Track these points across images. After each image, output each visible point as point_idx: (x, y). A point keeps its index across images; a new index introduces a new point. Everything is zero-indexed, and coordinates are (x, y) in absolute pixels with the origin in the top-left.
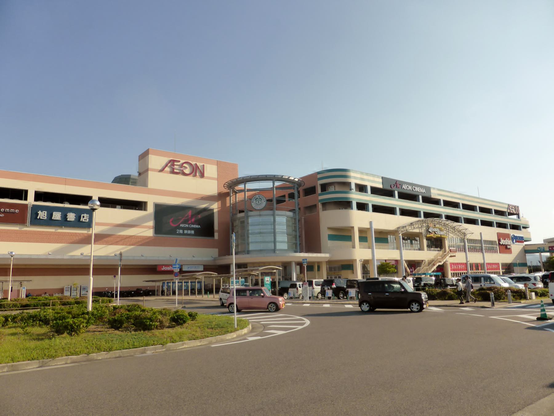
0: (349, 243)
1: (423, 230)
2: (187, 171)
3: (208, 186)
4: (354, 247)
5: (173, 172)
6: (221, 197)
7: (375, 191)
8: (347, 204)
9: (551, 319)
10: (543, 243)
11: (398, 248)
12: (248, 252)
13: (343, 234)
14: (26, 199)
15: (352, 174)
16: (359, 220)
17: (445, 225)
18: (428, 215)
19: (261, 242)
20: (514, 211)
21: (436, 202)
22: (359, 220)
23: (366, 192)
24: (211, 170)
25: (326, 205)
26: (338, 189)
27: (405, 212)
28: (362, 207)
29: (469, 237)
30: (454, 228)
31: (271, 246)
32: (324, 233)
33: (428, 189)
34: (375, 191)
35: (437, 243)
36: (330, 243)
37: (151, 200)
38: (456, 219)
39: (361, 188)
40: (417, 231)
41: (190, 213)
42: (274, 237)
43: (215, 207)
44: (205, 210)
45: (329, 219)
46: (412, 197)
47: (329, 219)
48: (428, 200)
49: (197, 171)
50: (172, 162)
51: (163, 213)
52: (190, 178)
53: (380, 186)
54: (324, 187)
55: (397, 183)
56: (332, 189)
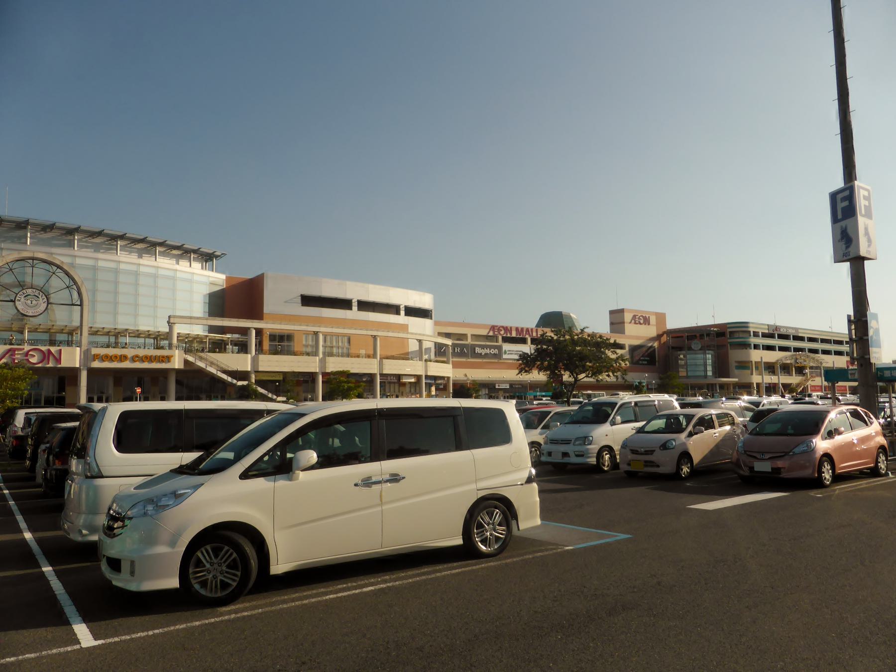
0: (749, 372)
1: (793, 361)
2: (642, 322)
3: (651, 331)
4: (752, 374)
5: (635, 323)
6: (659, 337)
7: (765, 335)
8: (746, 346)
9: (658, 466)
10: (770, 470)
11: (761, 374)
12: (408, 333)
13: (744, 365)
14: (467, 340)
15: (751, 325)
16: (756, 356)
17: (808, 356)
18: (797, 350)
19: (345, 304)
21: (801, 339)
22: (756, 356)
23: (758, 336)
24: (653, 320)
26: (741, 335)
27: (782, 349)
28: (756, 347)
29: (824, 365)
30: (813, 359)
31: (702, 374)
32: (733, 364)
33: (796, 329)
34: (765, 335)
35: (800, 370)
36: (737, 372)
37: (627, 342)
38: (815, 351)
39: (756, 334)
40: (789, 362)
41: (644, 349)
42: (704, 363)
43: (656, 344)
44: (651, 347)
45: (735, 355)
47: (735, 355)
48: (797, 338)
49: (647, 321)
50: (634, 316)
51: (634, 349)
52: (643, 326)
53: (767, 331)
54: (731, 332)
55: (777, 328)
56: (737, 335)
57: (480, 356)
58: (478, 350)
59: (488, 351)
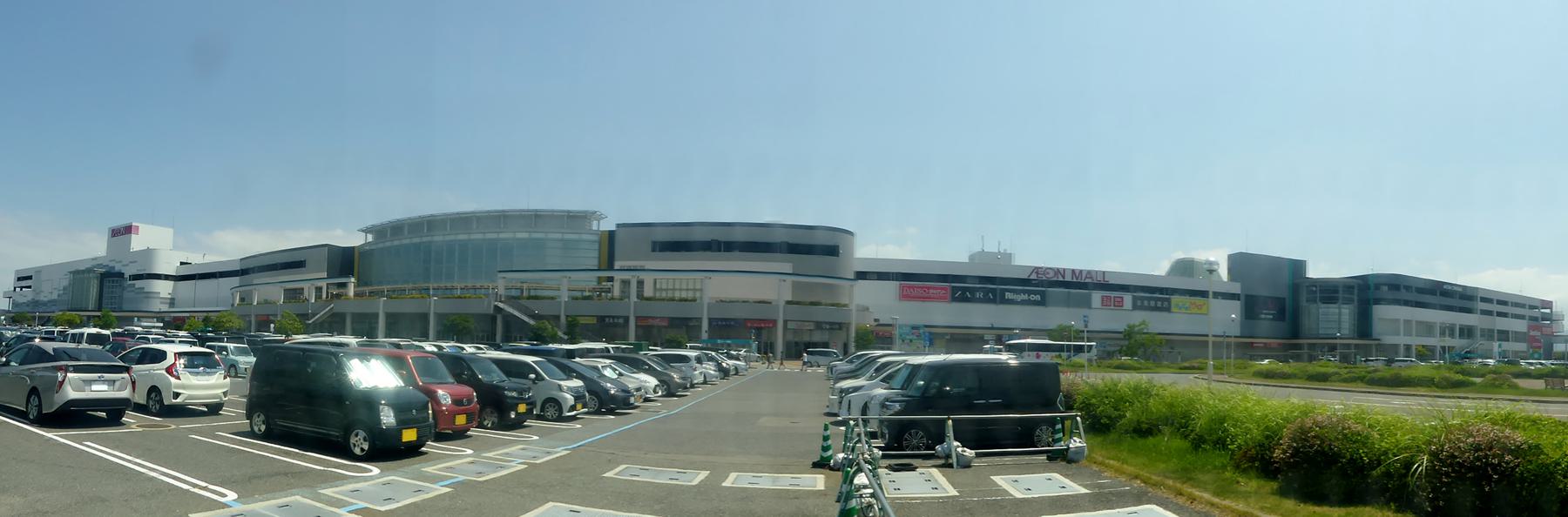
20: (1548, 305)
25: (1378, 301)
46: (1523, 306)
47: (1385, 314)
58: (1008, 295)
59: (1025, 297)
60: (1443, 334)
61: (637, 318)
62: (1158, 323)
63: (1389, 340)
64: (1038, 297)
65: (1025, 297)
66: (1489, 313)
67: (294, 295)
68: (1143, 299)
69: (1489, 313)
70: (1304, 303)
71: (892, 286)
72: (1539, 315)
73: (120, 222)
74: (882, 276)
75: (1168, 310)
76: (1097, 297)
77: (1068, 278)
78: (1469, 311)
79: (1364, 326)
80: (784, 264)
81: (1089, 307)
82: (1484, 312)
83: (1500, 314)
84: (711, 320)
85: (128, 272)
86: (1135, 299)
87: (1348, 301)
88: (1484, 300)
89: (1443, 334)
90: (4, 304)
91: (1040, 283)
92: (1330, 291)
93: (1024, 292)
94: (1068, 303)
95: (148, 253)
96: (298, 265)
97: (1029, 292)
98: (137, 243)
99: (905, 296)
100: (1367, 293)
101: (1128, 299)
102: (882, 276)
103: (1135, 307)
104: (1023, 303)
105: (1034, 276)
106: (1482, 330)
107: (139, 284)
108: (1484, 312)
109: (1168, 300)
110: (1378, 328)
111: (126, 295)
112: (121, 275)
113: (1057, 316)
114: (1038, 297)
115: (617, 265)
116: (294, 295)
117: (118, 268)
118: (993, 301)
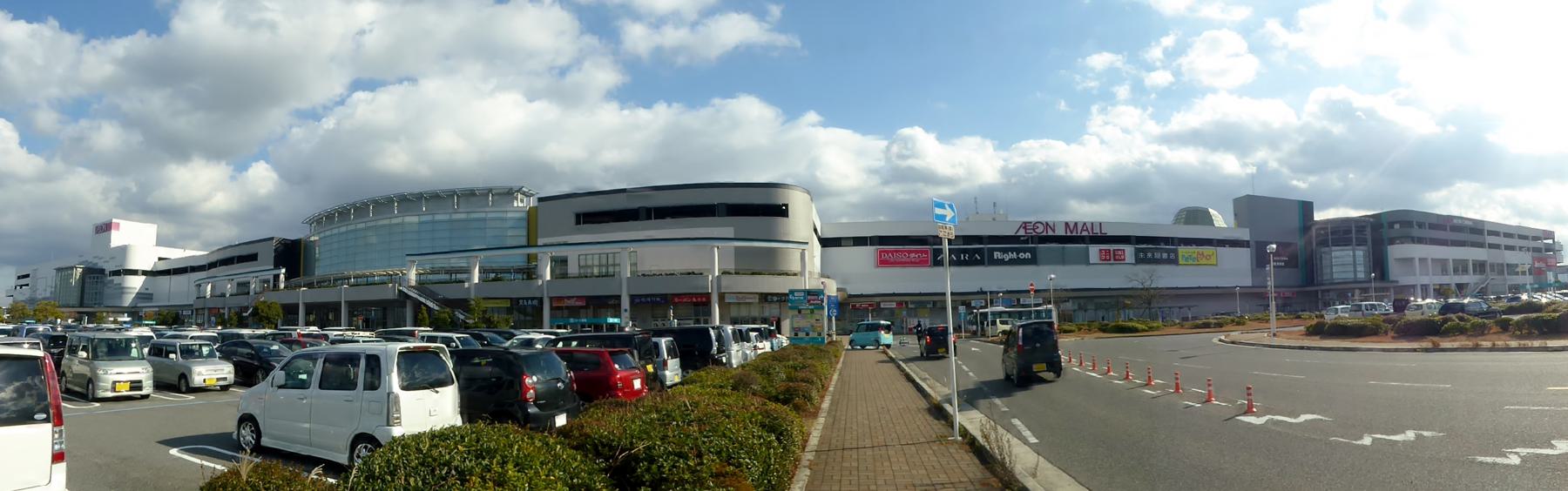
20: (1550, 235)
25: (1392, 242)
39: (1420, 225)
46: (1497, 234)
47: (1396, 252)
57: (1001, 262)
58: (997, 255)
59: (1014, 255)
60: (1456, 271)
61: (551, 299)
62: (1166, 277)
63: (1405, 280)
64: (1028, 255)
65: (1014, 255)
66: (1497, 247)
67: (243, 287)
68: (1142, 250)
69: (1497, 247)
70: (988, 474)
71: (869, 252)
72: (1541, 246)
73: (101, 220)
74: (859, 241)
75: (1175, 262)
76: (1094, 250)
77: (1060, 232)
78: (1481, 245)
79: (1379, 265)
80: (724, 228)
81: (1087, 262)
82: (1491, 246)
83: (1508, 248)
84: (633, 297)
85: (109, 267)
86: (1137, 251)
87: (1361, 242)
88: (1491, 233)
89: (1456, 271)
90: (6, 303)
91: (1032, 239)
92: (1343, 232)
93: (1012, 250)
94: (1063, 260)
95: (123, 250)
96: (252, 257)
97: (1018, 251)
98: (116, 239)
99: (883, 263)
100: (1379, 234)
101: (1129, 250)
102: (859, 241)
103: (1139, 261)
104: (1012, 262)
105: (1022, 232)
106: (1492, 266)
107: (116, 279)
108: (1491, 246)
109: (1176, 252)
110: (1396, 272)
111: (107, 291)
112: (102, 271)
113: (1052, 276)
114: (1028, 255)
115: (541, 241)
116: (243, 287)
117: (101, 264)
118: (980, 263)
